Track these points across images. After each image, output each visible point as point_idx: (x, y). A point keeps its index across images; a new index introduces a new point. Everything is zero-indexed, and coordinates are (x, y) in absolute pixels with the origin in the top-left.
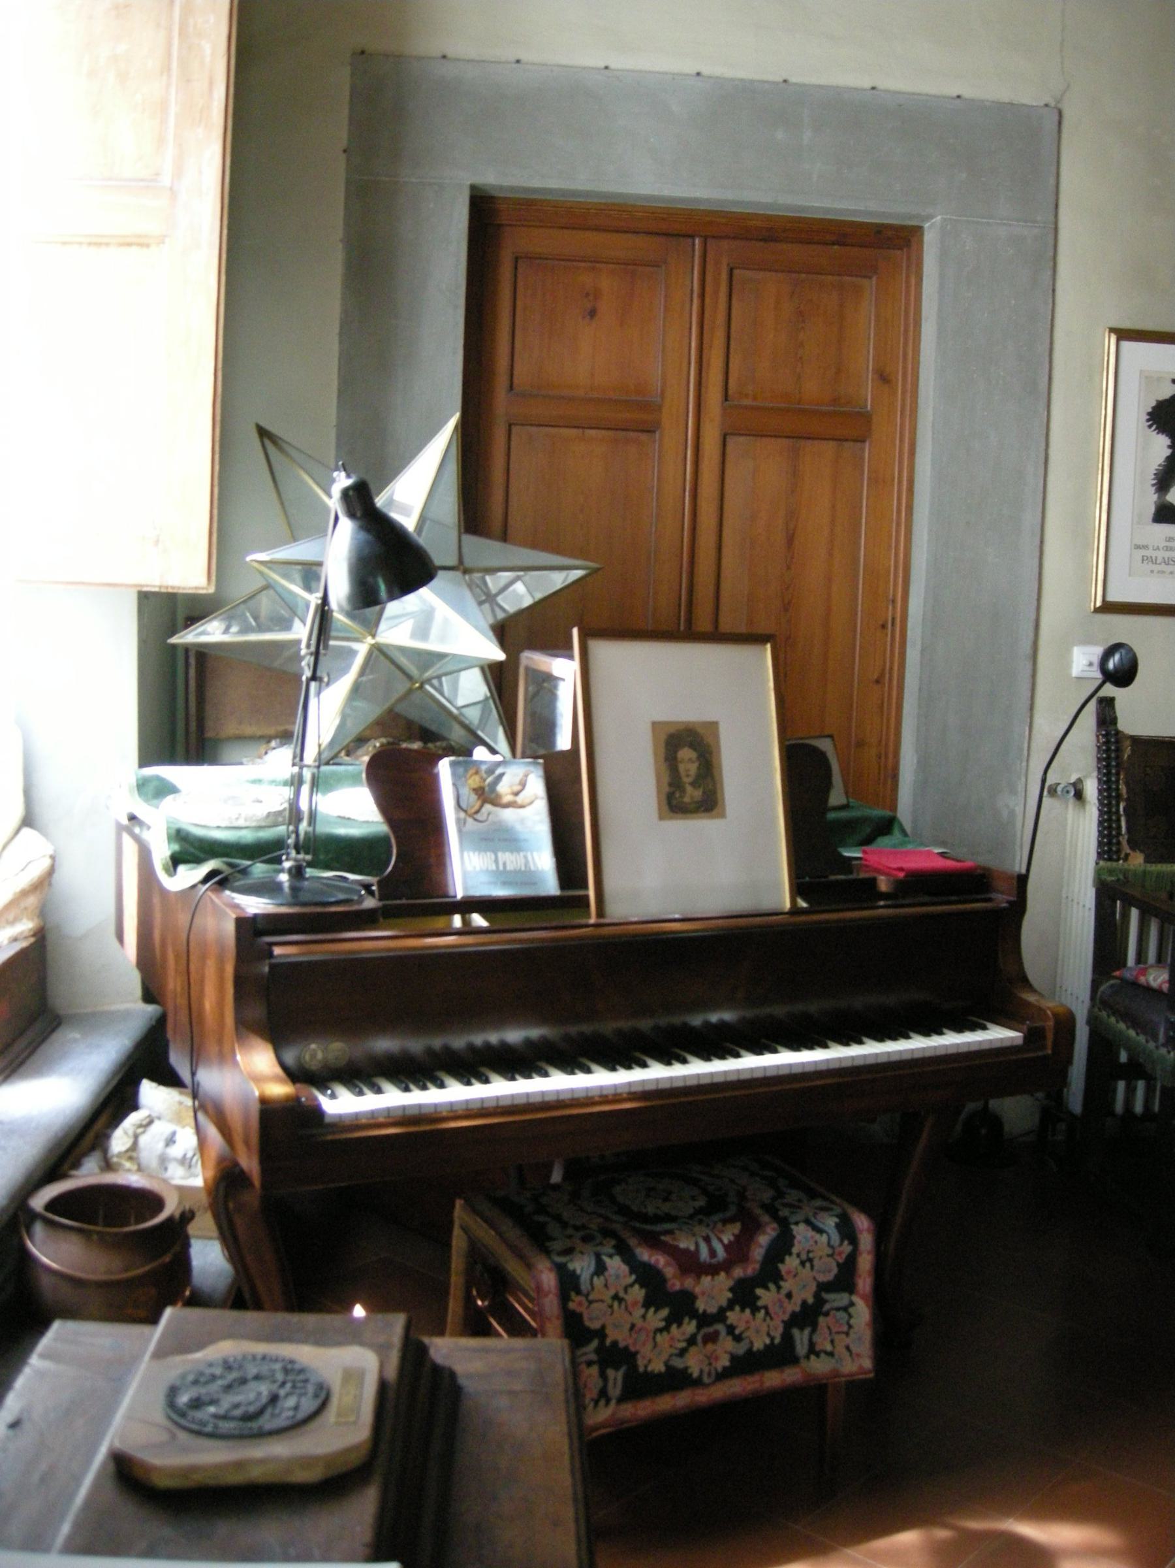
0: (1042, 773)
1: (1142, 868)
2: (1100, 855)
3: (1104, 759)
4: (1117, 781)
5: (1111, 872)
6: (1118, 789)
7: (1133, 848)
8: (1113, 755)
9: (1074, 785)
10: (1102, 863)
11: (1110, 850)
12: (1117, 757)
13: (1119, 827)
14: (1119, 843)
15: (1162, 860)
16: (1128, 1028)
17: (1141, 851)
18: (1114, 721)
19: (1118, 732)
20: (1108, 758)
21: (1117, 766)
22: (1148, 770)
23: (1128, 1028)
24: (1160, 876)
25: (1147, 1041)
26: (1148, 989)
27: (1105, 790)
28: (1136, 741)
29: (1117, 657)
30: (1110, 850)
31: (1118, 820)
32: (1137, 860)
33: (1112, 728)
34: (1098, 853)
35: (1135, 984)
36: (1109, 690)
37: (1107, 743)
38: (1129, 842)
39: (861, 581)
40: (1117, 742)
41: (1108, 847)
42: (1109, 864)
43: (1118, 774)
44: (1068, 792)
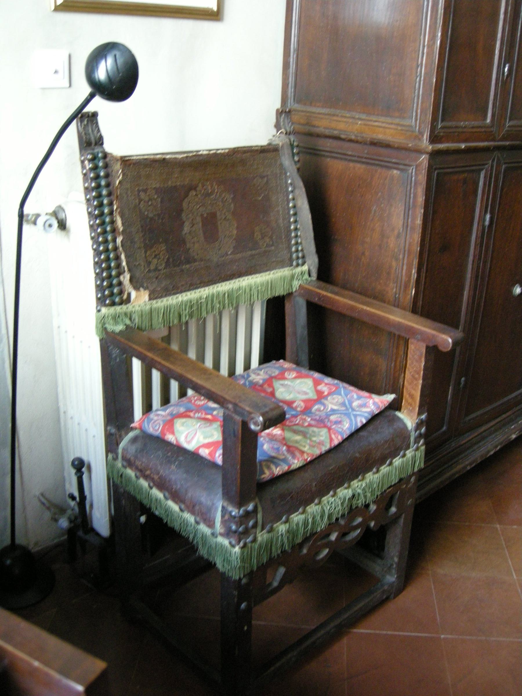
0: (18, 207)
1: (148, 307)
2: (101, 301)
3: (93, 189)
4: (111, 213)
5: (116, 318)
6: (113, 222)
7: (137, 288)
8: (103, 183)
9: (55, 214)
10: (104, 310)
11: (112, 294)
12: (108, 185)
13: (119, 266)
14: (120, 284)
15: (168, 292)
16: (166, 498)
17: (145, 289)
18: (100, 141)
19: (105, 155)
20: (98, 186)
21: (109, 195)
22: (142, 195)
23: (166, 498)
24: (167, 310)
25: (197, 523)
26: (179, 450)
27: (99, 225)
28: (125, 161)
29: (110, 60)
30: (112, 294)
31: (117, 258)
32: (140, 300)
33: (97, 150)
34: (98, 299)
35: (159, 441)
36: (99, 104)
37: (95, 168)
38: (131, 280)
39: (447, 55)
40: (106, 166)
41: (109, 292)
42: (112, 310)
43: (111, 204)
44: (50, 226)
